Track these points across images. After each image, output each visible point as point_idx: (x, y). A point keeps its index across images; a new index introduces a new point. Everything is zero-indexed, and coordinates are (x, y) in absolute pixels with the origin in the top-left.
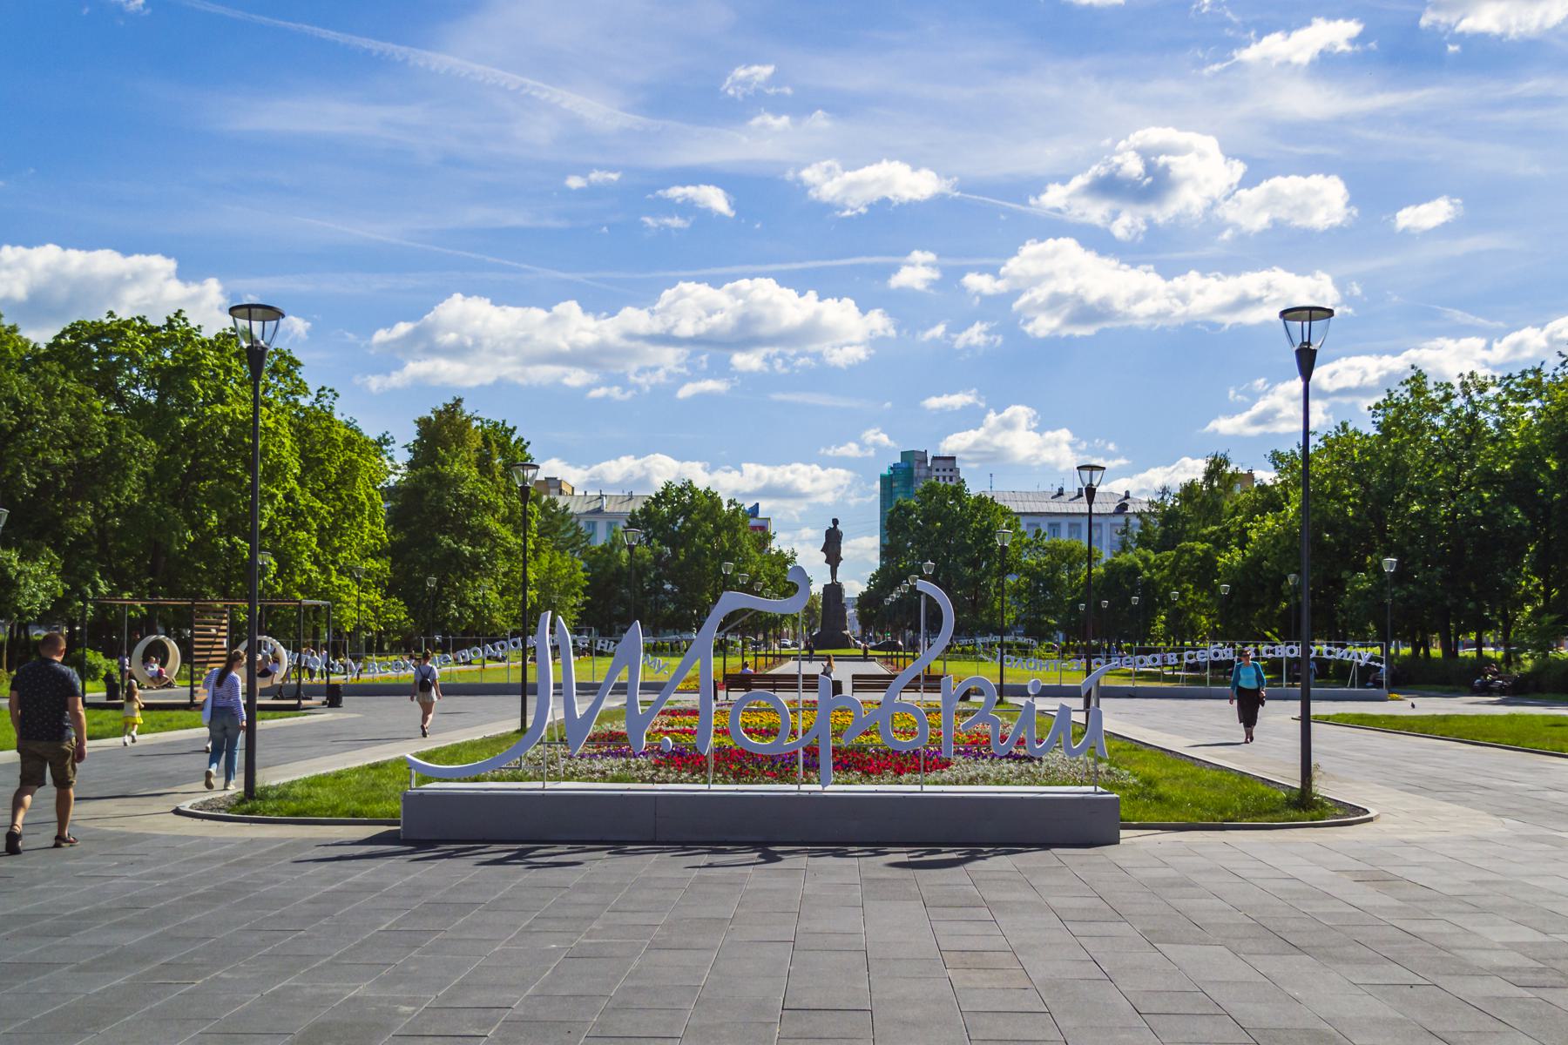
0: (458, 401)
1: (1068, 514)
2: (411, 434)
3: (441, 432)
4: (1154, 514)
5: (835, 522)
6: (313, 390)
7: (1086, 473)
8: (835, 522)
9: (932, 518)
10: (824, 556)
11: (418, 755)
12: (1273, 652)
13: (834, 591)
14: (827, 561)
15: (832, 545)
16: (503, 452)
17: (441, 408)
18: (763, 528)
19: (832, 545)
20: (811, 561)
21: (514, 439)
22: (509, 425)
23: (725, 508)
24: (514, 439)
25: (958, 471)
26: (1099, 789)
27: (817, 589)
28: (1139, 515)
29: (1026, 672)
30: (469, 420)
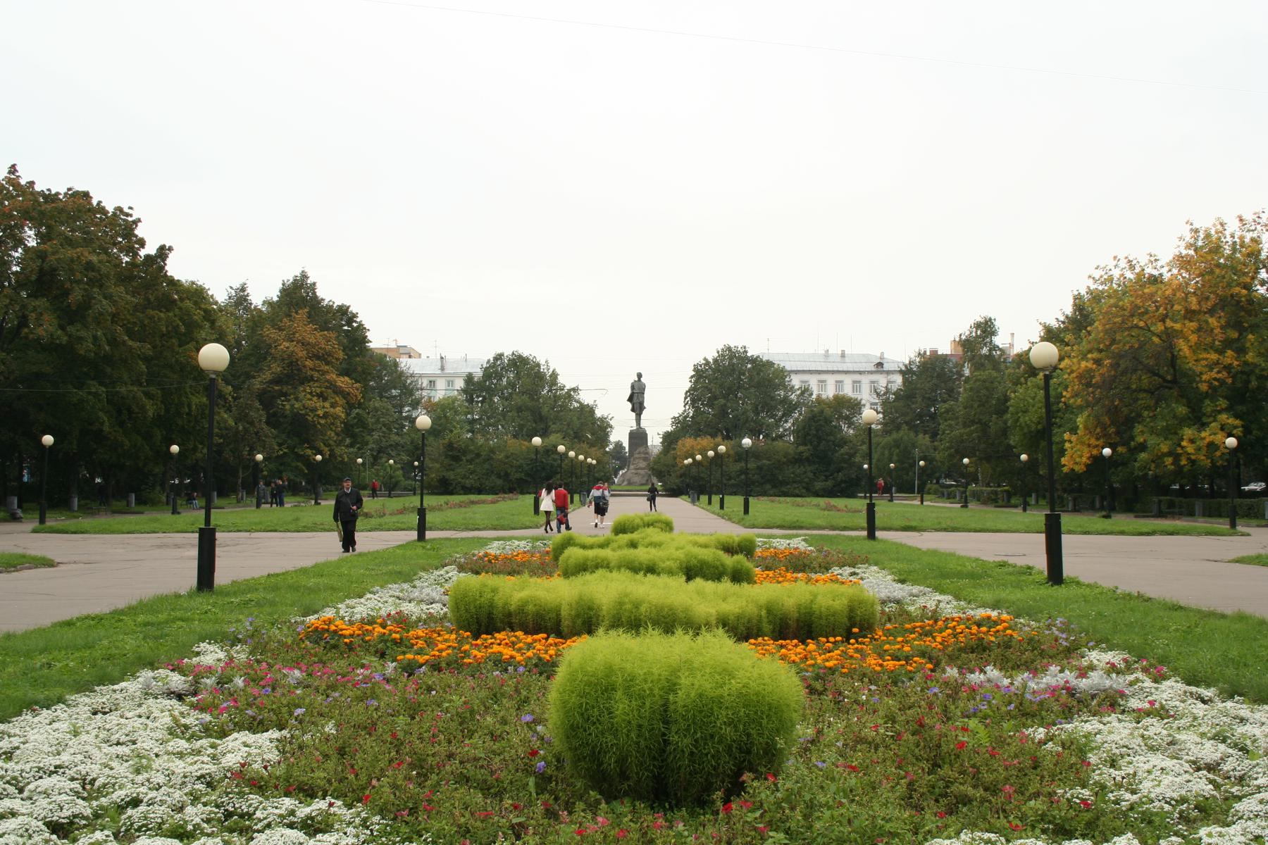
1: (833, 372)
5: (640, 376)
8: (640, 376)
10: (629, 405)
13: (638, 437)
14: (633, 410)
15: (637, 400)
19: (637, 400)
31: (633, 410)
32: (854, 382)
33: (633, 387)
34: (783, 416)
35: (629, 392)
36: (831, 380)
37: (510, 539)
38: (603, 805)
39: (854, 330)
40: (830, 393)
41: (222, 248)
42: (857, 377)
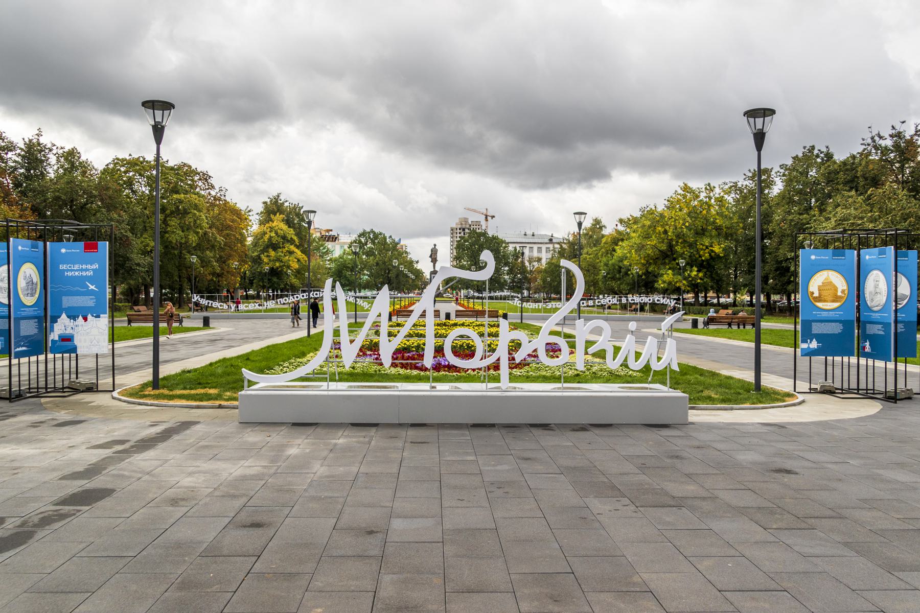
2: (260, 208)
3: (274, 208)
6: (217, 187)
7: (577, 216)
19: (434, 258)
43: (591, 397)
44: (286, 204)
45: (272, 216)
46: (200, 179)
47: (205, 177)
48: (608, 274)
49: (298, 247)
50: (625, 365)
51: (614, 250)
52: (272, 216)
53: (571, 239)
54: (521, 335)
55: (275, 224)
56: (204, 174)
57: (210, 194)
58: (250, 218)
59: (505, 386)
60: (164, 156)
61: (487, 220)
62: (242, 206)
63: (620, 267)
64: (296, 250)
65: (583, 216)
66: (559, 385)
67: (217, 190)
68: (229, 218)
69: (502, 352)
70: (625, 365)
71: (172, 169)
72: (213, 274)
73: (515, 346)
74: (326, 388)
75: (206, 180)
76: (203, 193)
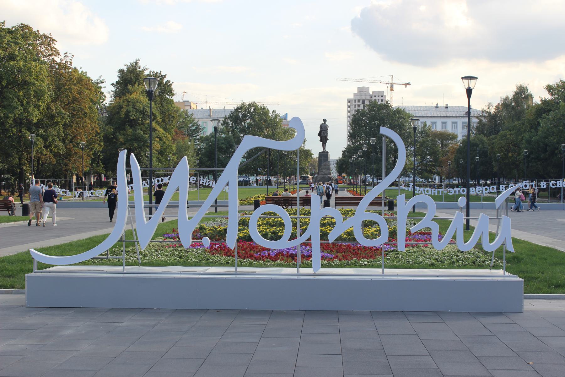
0: (137, 63)
1: (440, 117)
2: (116, 78)
3: (130, 78)
4: (485, 117)
5: (325, 121)
6: (62, 53)
7: (466, 81)
8: (325, 121)
9: (372, 118)
10: (319, 138)
11: (105, 237)
12: (556, 184)
13: (324, 155)
14: (321, 141)
15: (323, 135)
16: (161, 88)
17: (129, 64)
18: (300, 151)
19: (323, 135)
20: (314, 147)
21: (165, 80)
22: (163, 74)
23: (270, 115)
24: (165, 80)
25: (385, 97)
26: (507, 273)
27: (316, 155)
28: (477, 117)
29: (520, 184)
30: (142, 71)
31: (321, 141)
32: (453, 123)
33: (321, 127)
34: (27, 29)
35: (319, 130)
36: (439, 121)
37: (314, 275)
38: (158, 189)
39: (445, 89)
40: (439, 128)
41: (95, 52)
42: (455, 120)
43: (371, 280)
44: (147, 72)
45: (130, 87)
46: (42, 44)
47: (48, 41)
48: (531, 153)
49: (159, 124)
50: (479, 246)
51: (539, 124)
52: (130, 87)
53: (492, 112)
54: (333, 211)
55: (133, 96)
56: (47, 38)
57: (53, 60)
58: (102, 90)
59: (317, 271)
60: (473, 107)
61: (392, 90)
62: (93, 76)
63: (546, 145)
64: (158, 128)
65: (472, 81)
66: (232, 269)
67: (62, 56)
68: (71, 86)
69: (314, 231)
70: (479, 246)
71: (9, 31)
72: (56, 155)
73: (327, 223)
74: (381, 273)
75: (50, 44)
76: (45, 59)
